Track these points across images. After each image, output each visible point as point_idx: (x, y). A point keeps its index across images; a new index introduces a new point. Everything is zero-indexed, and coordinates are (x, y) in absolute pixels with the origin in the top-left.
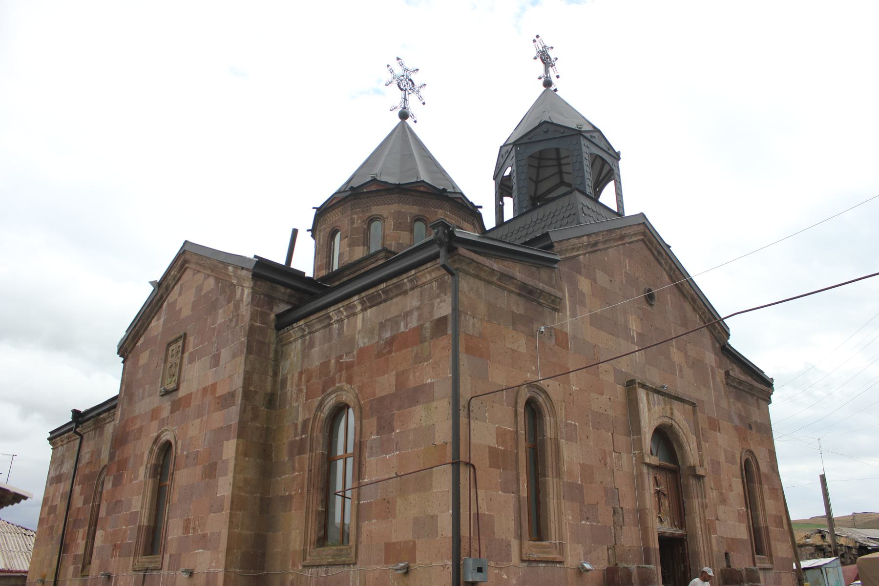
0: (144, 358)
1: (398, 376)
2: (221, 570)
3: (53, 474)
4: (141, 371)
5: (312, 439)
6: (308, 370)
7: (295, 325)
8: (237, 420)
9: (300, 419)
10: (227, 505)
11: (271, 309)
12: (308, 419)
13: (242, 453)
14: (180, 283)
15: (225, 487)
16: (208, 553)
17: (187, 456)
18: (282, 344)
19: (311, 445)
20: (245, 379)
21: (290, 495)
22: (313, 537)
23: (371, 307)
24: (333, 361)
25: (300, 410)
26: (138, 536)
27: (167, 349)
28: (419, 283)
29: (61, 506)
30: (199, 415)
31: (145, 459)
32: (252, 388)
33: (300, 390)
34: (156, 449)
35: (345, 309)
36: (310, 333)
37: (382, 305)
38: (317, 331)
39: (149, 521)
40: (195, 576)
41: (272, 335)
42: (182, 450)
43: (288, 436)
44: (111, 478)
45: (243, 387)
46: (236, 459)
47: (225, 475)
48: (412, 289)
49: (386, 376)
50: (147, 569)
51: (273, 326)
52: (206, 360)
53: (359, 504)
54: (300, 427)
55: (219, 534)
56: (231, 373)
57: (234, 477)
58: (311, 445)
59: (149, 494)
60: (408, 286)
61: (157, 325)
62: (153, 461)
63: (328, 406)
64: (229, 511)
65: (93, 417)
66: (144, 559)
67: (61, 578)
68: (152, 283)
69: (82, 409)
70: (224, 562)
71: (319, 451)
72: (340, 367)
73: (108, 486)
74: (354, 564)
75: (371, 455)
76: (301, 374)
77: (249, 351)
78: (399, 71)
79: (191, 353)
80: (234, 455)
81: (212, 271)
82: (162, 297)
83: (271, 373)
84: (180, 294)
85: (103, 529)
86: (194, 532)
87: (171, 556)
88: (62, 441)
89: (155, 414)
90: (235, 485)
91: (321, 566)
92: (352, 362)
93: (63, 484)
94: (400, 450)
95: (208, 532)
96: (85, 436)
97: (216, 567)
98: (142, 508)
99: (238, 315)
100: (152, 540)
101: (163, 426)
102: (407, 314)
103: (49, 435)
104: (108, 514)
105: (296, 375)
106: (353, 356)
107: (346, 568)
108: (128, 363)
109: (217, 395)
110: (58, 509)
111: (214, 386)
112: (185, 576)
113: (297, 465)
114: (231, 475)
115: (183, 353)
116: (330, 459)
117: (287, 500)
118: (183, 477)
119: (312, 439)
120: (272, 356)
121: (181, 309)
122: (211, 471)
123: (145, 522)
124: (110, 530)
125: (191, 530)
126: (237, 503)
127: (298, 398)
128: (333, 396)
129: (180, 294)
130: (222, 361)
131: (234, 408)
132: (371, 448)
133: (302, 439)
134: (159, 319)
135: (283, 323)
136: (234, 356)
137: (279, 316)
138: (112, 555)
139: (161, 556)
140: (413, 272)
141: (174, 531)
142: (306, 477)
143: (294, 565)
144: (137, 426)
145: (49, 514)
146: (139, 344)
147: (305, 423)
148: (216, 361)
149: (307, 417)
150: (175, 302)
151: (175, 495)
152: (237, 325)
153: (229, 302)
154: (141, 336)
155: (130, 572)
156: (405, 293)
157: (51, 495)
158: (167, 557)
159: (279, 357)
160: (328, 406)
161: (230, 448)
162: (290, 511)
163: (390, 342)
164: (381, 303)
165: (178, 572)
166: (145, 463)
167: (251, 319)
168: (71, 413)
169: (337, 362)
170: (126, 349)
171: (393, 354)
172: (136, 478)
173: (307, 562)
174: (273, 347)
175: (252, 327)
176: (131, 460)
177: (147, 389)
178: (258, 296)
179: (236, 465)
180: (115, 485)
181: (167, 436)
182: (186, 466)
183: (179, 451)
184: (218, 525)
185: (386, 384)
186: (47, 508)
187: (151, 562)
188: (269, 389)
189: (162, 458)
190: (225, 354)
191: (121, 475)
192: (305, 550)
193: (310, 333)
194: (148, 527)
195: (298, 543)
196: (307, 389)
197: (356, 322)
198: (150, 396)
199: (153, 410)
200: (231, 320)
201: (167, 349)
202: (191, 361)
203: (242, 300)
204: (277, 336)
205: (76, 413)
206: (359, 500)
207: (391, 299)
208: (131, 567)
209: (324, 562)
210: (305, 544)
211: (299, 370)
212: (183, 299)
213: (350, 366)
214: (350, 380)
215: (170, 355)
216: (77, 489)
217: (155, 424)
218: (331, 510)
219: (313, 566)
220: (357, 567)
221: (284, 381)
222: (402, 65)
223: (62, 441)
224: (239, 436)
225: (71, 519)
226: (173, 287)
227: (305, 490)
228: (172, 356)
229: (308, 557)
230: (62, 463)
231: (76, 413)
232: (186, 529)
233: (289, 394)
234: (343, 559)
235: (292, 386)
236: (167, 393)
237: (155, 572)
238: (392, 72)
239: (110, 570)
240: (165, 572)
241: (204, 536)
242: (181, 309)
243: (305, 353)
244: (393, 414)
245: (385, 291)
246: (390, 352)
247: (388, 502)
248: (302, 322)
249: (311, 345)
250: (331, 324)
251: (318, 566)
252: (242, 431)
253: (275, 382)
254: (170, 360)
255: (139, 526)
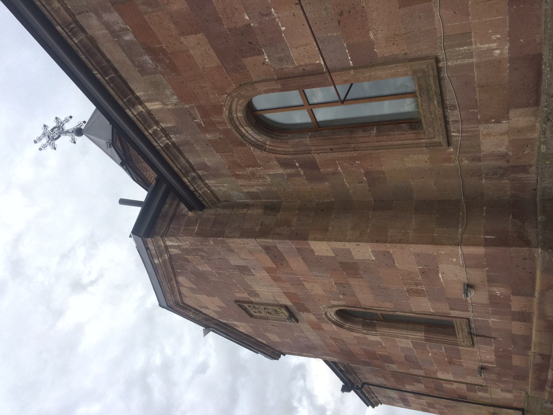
0: (273, 338)
1: (183, 33)
2: (459, 250)
3: (401, 404)
4: (286, 340)
5: (296, 153)
6: (229, 168)
7: (192, 188)
8: (289, 242)
9: (281, 171)
10: (382, 247)
11: (185, 215)
12: (278, 160)
13: (325, 235)
14: (199, 309)
15: (363, 252)
16: (443, 267)
17: (344, 294)
18: (216, 201)
19: (304, 152)
20: (247, 237)
21: (367, 174)
22: (408, 137)
23: (133, 93)
24: (208, 136)
25: (270, 174)
26: (437, 342)
27: (256, 317)
28: (70, 19)
29: (424, 400)
30: (299, 284)
31: (360, 335)
32: (257, 229)
33: (253, 174)
34: (347, 325)
35: (150, 127)
36: (194, 171)
37: (124, 75)
38: (188, 161)
39: (420, 331)
40: (472, 282)
41: (209, 213)
42: (339, 300)
43: (302, 185)
44: (386, 365)
45: (256, 237)
46: (329, 240)
47: (349, 251)
48: (83, 30)
49: (192, 52)
50: (470, 334)
51: (200, 213)
52: (248, 279)
53: (354, 68)
54: (289, 171)
55: (418, 255)
56: (245, 251)
57: (350, 241)
58: (304, 152)
59: (393, 331)
60: (82, 36)
61: (243, 327)
62: (359, 327)
63: (256, 136)
64: (388, 245)
65: (344, 375)
66: (460, 336)
67: (489, 401)
68: (205, 333)
69: (341, 384)
70: (450, 248)
71: (307, 141)
72: (210, 126)
73: (394, 367)
74: (437, 61)
75: (288, 58)
76: (238, 177)
77: (221, 234)
78: (45, 140)
79: (249, 294)
80: (325, 243)
81: (171, 280)
82: (216, 324)
83: (245, 211)
84: (207, 308)
85: (436, 373)
86: (420, 284)
87: (451, 309)
88: (373, 398)
89: (316, 327)
90: (358, 240)
91: (445, 117)
92: (200, 108)
93: (408, 398)
94: (269, 8)
95: (416, 268)
96: (363, 381)
97: (457, 256)
98: (407, 338)
99: (194, 250)
100: (438, 327)
101: (323, 319)
102: (107, 26)
103: (370, 407)
104: (420, 368)
105: (241, 182)
106: (192, 107)
107: (445, 74)
108: (284, 351)
109: (275, 266)
110: (429, 402)
111: (268, 270)
112: (472, 294)
113: (330, 170)
114: (348, 245)
115: (252, 303)
116: (317, 128)
117: (374, 178)
118: (365, 298)
119: (296, 153)
120: (227, 212)
121: (218, 306)
122: (351, 268)
123: (420, 336)
124: (435, 367)
125: (419, 287)
126: (378, 237)
127: (260, 177)
128: (244, 132)
129: (207, 308)
130: (242, 263)
131: (279, 246)
132: (281, 60)
133: (301, 166)
134: (237, 326)
135: (196, 203)
136: (231, 251)
137: (191, 209)
138: (460, 365)
139: (454, 320)
140: (59, 28)
141: (423, 306)
142: (340, 155)
143: (448, 160)
144: (333, 342)
145: (435, 408)
146: (264, 342)
147: (284, 164)
148: (244, 270)
149: (276, 163)
150: (215, 312)
151: (386, 306)
152: (202, 250)
153: (187, 261)
154: (257, 340)
155: (475, 349)
156: (92, 40)
157: (419, 406)
158: (454, 313)
159: (233, 205)
160: (256, 136)
161: (321, 248)
162: (383, 172)
163: (150, 51)
164: (120, 77)
165: (469, 301)
166: (364, 335)
167: (191, 235)
168: (345, 393)
169: (205, 130)
170: (274, 353)
171: (164, 46)
172: (379, 343)
173: (444, 141)
174: (220, 211)
175: (198, 234)
176: (365, 347)
177: (298, 334)
178: (170, 230)
179: (336, 240)
180: (392, 362)
181: (332, 314)
182: (354, 295)
183: (342, 303)
184: (407, 257)
185: (198, 49)
186: (431, 409)
187: (462, 329)
188: (260, 211)
189: (357, 319)
190: (234, 261)
191: (381, 356)
192: (427, 146)
193: (194, 171)
194: (425, 331)
195: (421, 157)
196: (249, 167)
197: (157, 110)
198: (303, 332)
199: (314, 328)
200: (202, 257)
201: (256, 317)
202: (256, 295)
203: (178, 247)
204: (211, 208)
205: (346, 389)
206: (350, 68)
207: (108, 61)
208: (470, 349)
209: (439, 111)
210: (418, 145)
211: (234, 179)
212: (212, 305)
213: (205, 112)
214: (218, 109)
215: (261, 315)
216: (408, 388)
217: (324, 326)
218: (377, 120)
219: (447, 131)
220: (441, 55)
221: (250, 195)
222: (40, 139)
223: (373, 398)
224: (306, 238)
225: (436, 393)
226: (205, 314)
227: (355, 154)
228: (260, 312)
229: (436, 140)
230: (390, 397)
231: (346, 389)
232: (419, 293)
233: (261, 188)
234: (432, 82)
235: (252, 186)
236: (292, 316)
237: (473, 326)
238: (45, 146)
239: (476, 367)
240: (470, 315)
241: (423, 273)
242: (218, 306)
243: (215, 174)
244: (230, 30)
245: (104, 73)
246: (163, 51)
247: (341, 14)
248: (185, 180)
249: (204, 166)
250: (173, 143)
251: (446, 123)
252: (300, 236)
253: (254, 205)
254: (263, 314)
255: (426, 340)
